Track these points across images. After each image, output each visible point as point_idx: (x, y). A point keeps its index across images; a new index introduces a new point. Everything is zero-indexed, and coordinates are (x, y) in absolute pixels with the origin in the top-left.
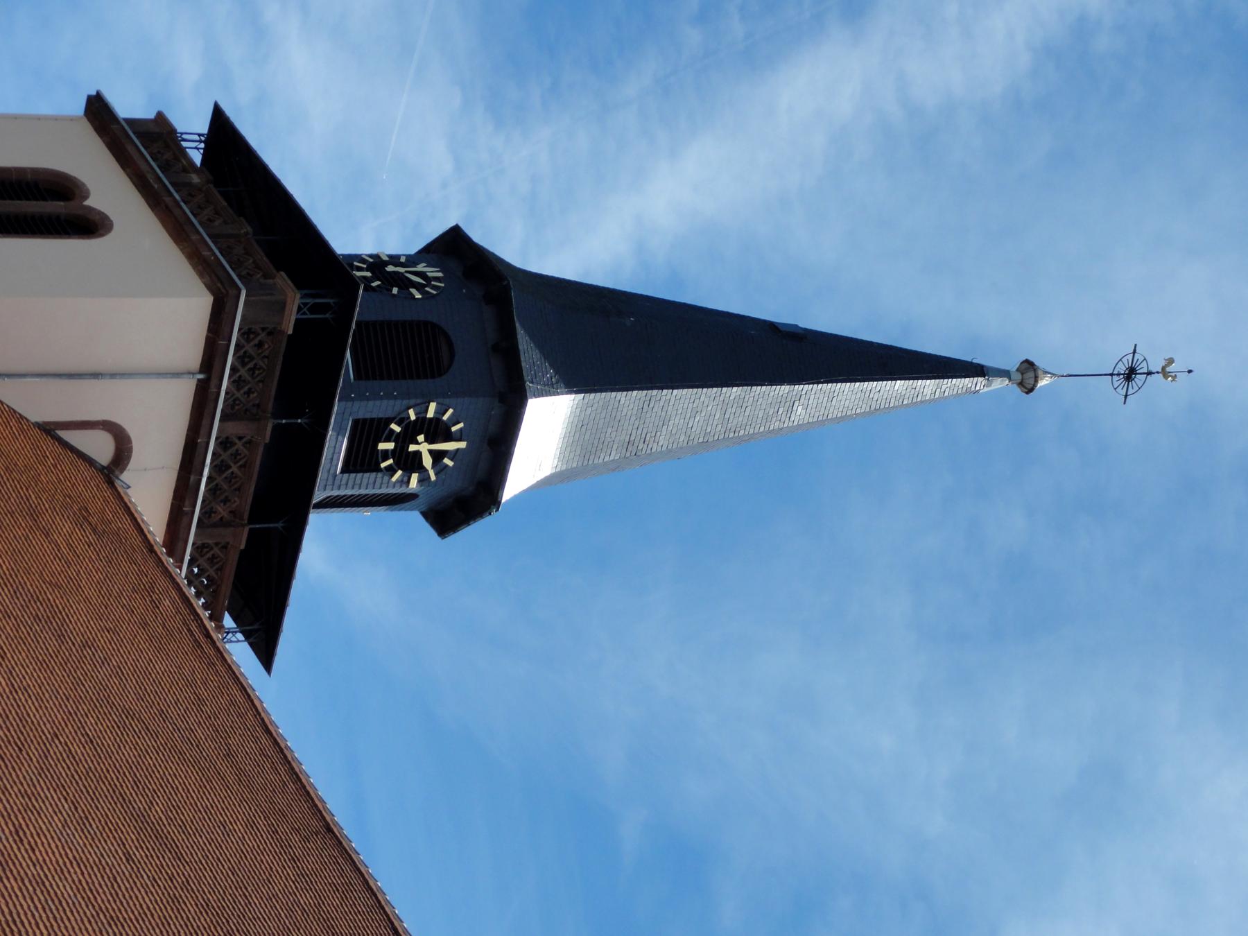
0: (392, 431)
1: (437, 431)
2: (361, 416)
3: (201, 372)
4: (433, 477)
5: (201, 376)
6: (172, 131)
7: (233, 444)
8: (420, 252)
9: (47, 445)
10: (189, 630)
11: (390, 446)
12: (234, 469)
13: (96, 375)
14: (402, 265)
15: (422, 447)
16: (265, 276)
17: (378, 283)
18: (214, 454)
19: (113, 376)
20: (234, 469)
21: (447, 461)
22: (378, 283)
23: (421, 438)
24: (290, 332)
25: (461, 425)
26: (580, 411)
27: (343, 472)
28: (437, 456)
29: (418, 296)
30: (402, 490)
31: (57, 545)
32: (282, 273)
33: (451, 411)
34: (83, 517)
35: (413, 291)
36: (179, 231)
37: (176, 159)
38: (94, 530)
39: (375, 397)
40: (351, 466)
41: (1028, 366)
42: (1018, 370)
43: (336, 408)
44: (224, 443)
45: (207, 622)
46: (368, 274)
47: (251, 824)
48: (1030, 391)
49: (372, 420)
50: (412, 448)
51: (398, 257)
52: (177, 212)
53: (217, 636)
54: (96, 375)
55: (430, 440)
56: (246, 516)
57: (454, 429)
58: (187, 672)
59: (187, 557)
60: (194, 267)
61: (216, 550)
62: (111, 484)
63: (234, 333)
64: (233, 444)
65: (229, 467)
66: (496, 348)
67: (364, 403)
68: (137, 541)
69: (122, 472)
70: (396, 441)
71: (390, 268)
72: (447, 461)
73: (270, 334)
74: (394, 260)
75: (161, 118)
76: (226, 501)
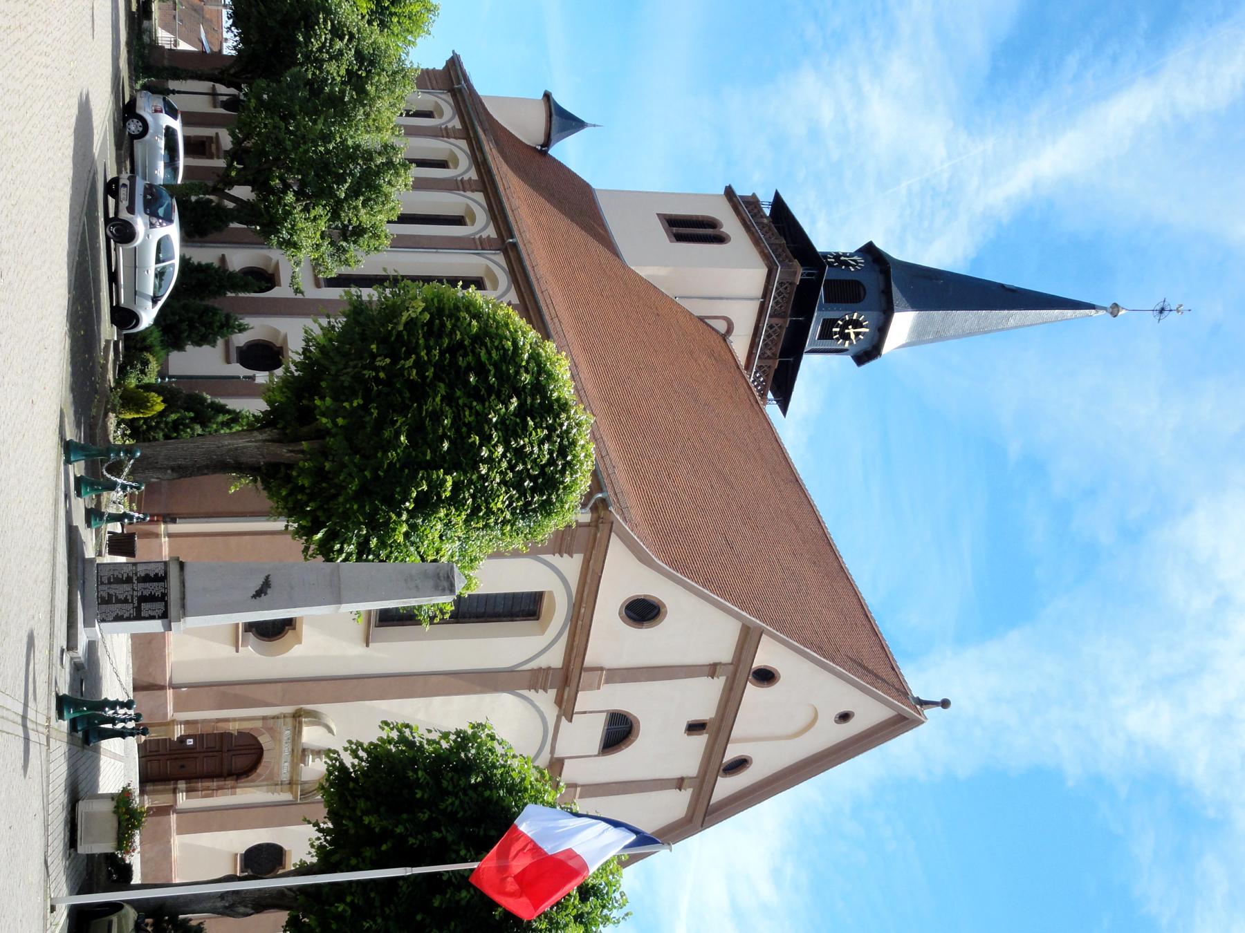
0: (839, 324)
1: (857, 324)
2: (826, 317)
3: (762, 298)
4: (855, 343)
5: (762, 300)
6: (758, 201)
7: (774, 327)
8: (856, 251)
9: (700, 324)
10: (750, 400)
11: (838, 330)
12: (774, 337)
13: (721, 298)
14: (848, 257)
15: (851, 331)
16: (790, 261)
17: (837, 264)
18: (766, 330)
19: (727, 299)
20: (774, 337)
21: (860, 336)
22: (837, 264)
23: (850, 327)
24: (798, 283)
25: (867, 322)
26: (919, 317)
27: (818, 339)
28: (857, 334)
29: (853, 270)
30: (842, 347)
31: (699, 365)
32: (796, 260)
33: (863, 317)
34: (712, 354)
35: (851, 267)
36: (756, 242)
37: (759, 212)
38: (715, 359)
39: (832, 310)
40: (822, 337)
41: (1116, 306)
42: (1111, 307)
43: (816, 314)
44: (771, 327)
45: (757, 397)
46: (833, 260)
47: (764, 477)
48: (1115, 316)
49: (831, 319)
50: (846, 331)
51: (846, 253)
52: (756, 234)
53: (761, 403)
54: (721, 298)
55: (854, 328)
56: (778, 355)
57: (864, 324)
58: (746, 416)
59: (754, 370)
60: (762, 257)
61: (765, 368)
62: (725, 340)
63: (103, 214)
64: (774, 327)
65: (772, 336)
66: (883, 292)
67: (828, 312)
68: (733, 364)
69: (730, 336)
70: (840, 328)
71: (842, 258)
72: (860, 336)
73: (790, 284)
74: (845, 255)
75: (754, 195)
76: (770, 349)
